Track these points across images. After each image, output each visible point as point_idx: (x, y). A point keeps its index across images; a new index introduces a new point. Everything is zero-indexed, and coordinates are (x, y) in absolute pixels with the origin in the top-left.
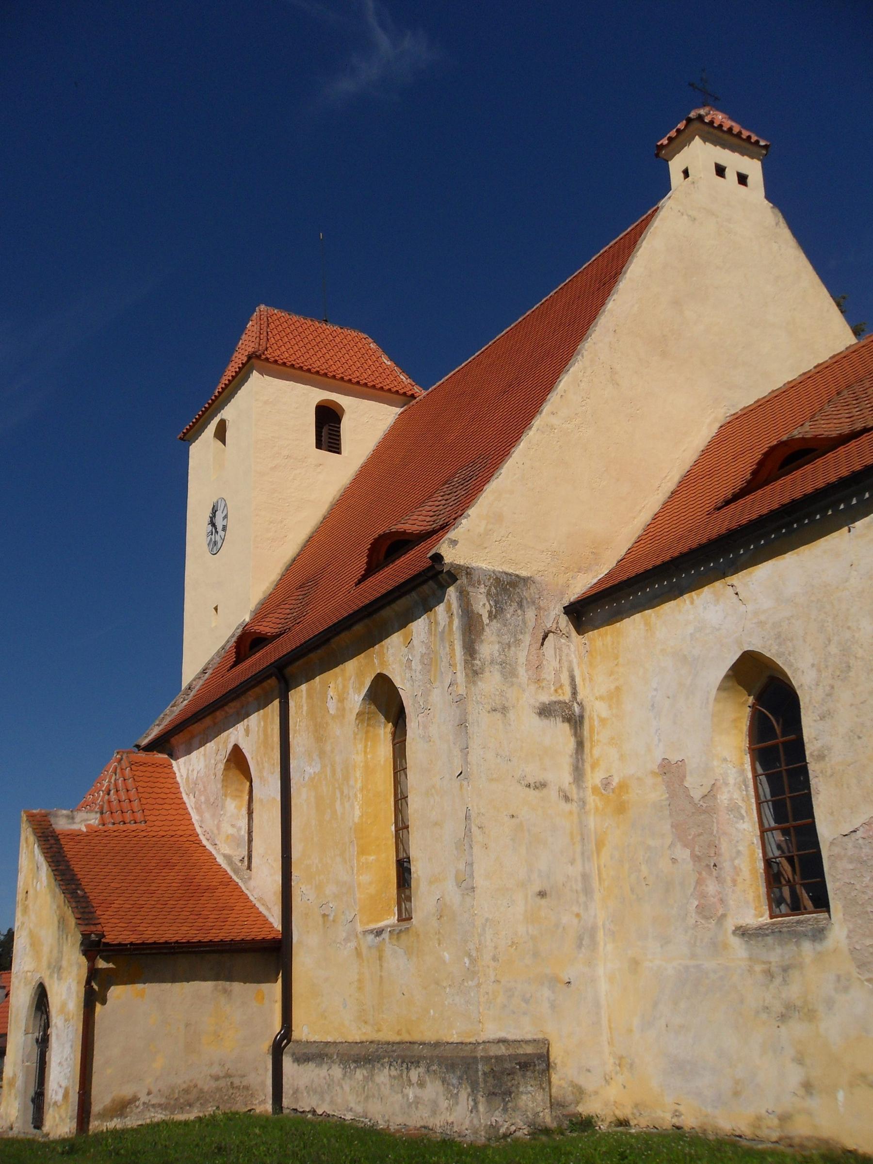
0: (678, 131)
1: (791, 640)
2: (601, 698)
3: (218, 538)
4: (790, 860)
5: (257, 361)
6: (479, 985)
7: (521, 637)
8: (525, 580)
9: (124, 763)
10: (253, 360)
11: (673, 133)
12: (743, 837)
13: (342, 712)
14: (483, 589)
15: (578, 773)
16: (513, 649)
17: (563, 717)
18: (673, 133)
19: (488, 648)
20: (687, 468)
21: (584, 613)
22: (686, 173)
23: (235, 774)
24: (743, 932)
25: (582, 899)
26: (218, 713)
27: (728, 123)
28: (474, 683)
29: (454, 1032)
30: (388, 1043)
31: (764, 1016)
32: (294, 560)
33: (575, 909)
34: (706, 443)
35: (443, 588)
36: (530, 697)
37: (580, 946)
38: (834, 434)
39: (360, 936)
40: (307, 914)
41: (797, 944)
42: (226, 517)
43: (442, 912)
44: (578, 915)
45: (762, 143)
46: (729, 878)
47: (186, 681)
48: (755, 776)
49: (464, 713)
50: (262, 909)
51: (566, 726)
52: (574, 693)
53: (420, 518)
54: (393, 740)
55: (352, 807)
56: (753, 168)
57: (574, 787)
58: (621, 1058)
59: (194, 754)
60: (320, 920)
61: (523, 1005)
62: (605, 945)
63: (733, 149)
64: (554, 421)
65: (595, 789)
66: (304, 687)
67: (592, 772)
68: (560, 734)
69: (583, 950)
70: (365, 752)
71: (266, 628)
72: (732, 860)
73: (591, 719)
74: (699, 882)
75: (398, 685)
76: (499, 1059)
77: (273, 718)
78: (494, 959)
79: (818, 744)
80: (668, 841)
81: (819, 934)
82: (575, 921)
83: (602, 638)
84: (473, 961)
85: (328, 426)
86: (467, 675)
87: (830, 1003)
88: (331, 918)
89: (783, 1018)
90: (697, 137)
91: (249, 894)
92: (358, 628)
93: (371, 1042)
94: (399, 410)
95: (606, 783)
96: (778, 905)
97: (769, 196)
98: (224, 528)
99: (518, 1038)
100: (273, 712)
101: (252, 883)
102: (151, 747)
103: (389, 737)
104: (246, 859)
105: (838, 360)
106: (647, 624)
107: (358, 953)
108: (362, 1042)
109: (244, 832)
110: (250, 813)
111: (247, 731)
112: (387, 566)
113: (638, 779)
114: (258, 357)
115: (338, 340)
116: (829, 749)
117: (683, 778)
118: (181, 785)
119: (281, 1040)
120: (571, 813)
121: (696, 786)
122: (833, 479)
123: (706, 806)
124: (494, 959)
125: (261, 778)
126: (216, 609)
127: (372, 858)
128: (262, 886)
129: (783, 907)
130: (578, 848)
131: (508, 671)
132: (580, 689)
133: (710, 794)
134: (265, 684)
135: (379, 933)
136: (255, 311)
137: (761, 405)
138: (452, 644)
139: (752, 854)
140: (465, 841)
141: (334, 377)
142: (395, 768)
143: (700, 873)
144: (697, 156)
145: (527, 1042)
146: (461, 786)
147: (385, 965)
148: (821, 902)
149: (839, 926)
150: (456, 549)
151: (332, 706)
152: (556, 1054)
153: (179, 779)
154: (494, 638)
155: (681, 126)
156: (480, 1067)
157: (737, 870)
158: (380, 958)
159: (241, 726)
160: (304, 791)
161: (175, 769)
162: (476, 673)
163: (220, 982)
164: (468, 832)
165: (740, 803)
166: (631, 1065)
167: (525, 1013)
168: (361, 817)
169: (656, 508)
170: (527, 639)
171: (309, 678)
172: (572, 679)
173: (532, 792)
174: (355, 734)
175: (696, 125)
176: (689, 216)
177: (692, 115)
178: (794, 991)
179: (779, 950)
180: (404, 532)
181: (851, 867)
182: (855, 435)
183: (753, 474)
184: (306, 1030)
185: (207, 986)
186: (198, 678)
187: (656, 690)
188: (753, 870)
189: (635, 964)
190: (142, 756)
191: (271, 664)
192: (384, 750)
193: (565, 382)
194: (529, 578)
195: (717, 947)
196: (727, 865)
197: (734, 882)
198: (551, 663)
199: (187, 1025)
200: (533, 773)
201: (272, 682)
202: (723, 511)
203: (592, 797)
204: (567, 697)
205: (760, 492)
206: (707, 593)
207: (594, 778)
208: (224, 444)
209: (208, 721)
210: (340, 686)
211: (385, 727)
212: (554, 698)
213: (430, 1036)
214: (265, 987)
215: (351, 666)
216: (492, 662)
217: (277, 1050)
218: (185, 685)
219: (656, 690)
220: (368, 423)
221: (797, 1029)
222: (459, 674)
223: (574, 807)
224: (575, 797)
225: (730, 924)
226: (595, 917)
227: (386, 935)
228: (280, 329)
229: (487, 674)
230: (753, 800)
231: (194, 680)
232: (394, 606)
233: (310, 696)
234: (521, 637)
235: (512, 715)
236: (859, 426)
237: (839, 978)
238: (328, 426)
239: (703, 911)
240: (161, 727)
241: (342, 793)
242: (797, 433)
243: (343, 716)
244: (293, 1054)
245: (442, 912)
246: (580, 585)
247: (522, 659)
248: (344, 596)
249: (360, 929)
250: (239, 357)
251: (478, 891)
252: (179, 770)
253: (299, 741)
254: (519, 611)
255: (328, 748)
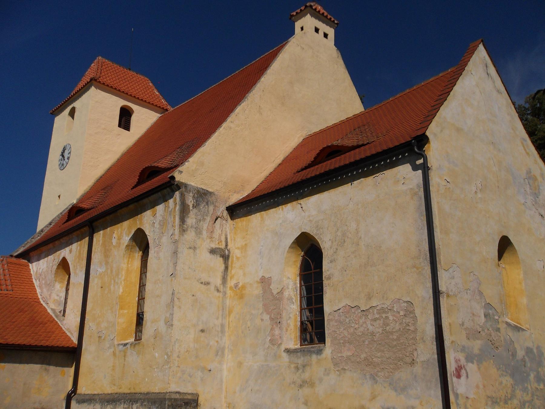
0: (301, 10)
1: (322, 228)
2: (238, 248)
3: (64, 163)
4: (311, 324)
5: (94, 82)
6: (170, 368)
7: (206, 217)
8: (211, 193)
9: (4, 262)
10: (93, 81)
11: (299, 11)
12: (292, 310)
13: (119, 244)
14: (191, 194)
15: (224, 280)
16: (202, 222)
17: (220, 255)
18: (299, 11)
19: (191, 220)
20: (287, 155)
21: (236, 211)
22: (302, 29)
23: (62, 272)
24: (288, 351)
25: (220, 335)
26: (56, 242)
27: (322, 11)
28: (183, 235)
29: (156, 388)
30: (124, 394)
31: (293, 386)
32: (101, 177)
33: (216, 339)
34: (296, 145)
35: (173, 191)
36: (206, 244)
37: (217, 355)
38: (350, 145)
39: (116, 346)
40: (91, 336)
41: (310, 356)
42: (70, 153)
43: (156, 335)
44: (217, 342)
45: (336, 22)
46: (284, 328)
47: (39, 229)
48: (301, 286)
49: (177, 248)
50: (68, 334)
51: (221, 259)
52: (227, 245)
53: (166, 161)
54: (142, 259)
55: (119, 288)
56: (331, 32)
57: (222, 286)
58: (229, 404)
59: (41, 261)
60: (97, 339)
61: (189, 378)
62: (228, 356)
63: (323, 22)
64: (232, 125)
65: (231, 288)
66: (101, 232)
67: (231, 280)
68: (219, 262)
69: (218, 357)
70: (128, 264)
71: (84, 206)
72: (287, 321)
73: (233, 257)
74: (272, 329)
75: (147, 234)
76: (176, 400)
77: (84, 245)
78: (178, 357)
79: (328, 273)
80: (261, 311)
81: (319, 352)
82: (216, 344)
83: (241, 222)
84: (169, 357)
85: (125, 118)
86: (180, 231)
87: (321, 380)
88: (103, 338)
89: (301, 386)
90: (309, 14)
91: (62, 327)
92: (131, 206)
93: (116, 394)
94: (159, 115)
95: (236, 286)
96: (304, 341)
97: (336, 45)
98: (68, 158)
99: (185, 392)
100: (85, 242)
101: (65, 322)
102: (19, 256)
103: (140, 257)
104: (62, 311)
105: (356, 117)
106: (262, 217)
107: (114, 354)
108: (111, 394)
109: (63, 299)
110: (67, 290)
111: (71, 251)
112: (148, 181)
113: (250, 284)
114: (96, 80)
115: (134, 79)
116: (333, 275)
117: (270, 285)
118: (33, 275)
119: (72, 393)
120: (219, 297)
121: (275, 288)
122: (347, 162)
123: (278, 298)
124: (178, 357)
125: (75, 273)
126: (59, 197)
127: (126, 311)
128: (70, 324)
129: (306, 343)
130: (221, 312)
131: (198, 231)
132: (229, 243)
133: (281, 292)
134: (82, 230)
135: (125, 345)
136: (96, 59)
137: (322, 132)
138: (174, 217)
139: (296, 319)
140: (171, 304)
141: (131, 95)
142: (141, 272)
143: (273, 326)
144: (308, 22)
145: (189, 394)
146: (172, 280)
147: (127, 359)
148: (322, 339)
149: (328, 349)
150: (180, 176)
151: (114, 241)
152: (201, 400)
153: (32, 272)
154: (193, 216)
155: (303, 8)
156: (167, 403)
157: (288, 325)
158: (125, 356)
159: (67, 249)
160: (96, 281)
161: (31, 267)
162: (184, 231)
163: (44, 365)
164: (173, 300)
165: (293, 297)
166: (234, 407)
167: (189, 382)
168: (123, 292)
169: (272, 170)
170: (208, 219)
171: (105, 228)
172: (226, 239)
173: (203, 286)
174: (124, 255)
175: (309, 9)
176: (301, 47)
177: (308, 4)
178: (306, 375)
179: (302, 358)
180: (157, 167)
181: (336, 324)
182: (358, 146)
183: (314, 158)
184: (84, 389)
185: (37, 367)
186: (47, 226)
187: (262, 246)
188: (295, 326)
189: (240, 364)
190: (14, 260)
191: (84, 221)
192: (137, 263)
193: (239, 109)
194: (212, 193)
195: (276, 357)
196: (284, 323)
197: (287, 330)
198: (217, 231)
199: (25, 384)
200: (205, 277)
201: (86, 229)
202: (300, 173)
203: (229, 292)
204: (223, 246)
205: (317, 166)
206: (289, 206)
207: (231, 283)
208: (73, 118)
209: (51, 245)
210: (119, 233)
211: (138, 253)
212: (217, 246)
213: (144, 390)
214: (66, 369)
215: (126, 224)
216: (192, 227)
217: (69, 399)
218: (38, 229)
219: (262, 246)
220: (144, 119)
221: (306, 391)
222: (176, 230)
223: (221, 295)
224: (222, 290)
225: (283, 348)
226: (225, 343)
227: (128, 346)
228: (107, 69)
229: (189, 232)
230: (299, 296)
231: (45, 227)
232: (149, 198)
233: (104, 236)
234: (206, 217)
235: (198, 251)
236: (361, 143)
237: (326, 369)
238: (125, 118)
239: (272, 342)
240: (25, 248)
241: (115, 281)
242: (335, 143)
243: (119, 247)
244: (77, 400)
245: (156, 335)
246: (235, 199)
247: (205, 227)
248: (124, 192)
249: (116, 343)
250: (86, 79)
251: (174, 326)
252: (33, 268)
253: (96, 257)
254: (206, 206)
255: (110, 260)
